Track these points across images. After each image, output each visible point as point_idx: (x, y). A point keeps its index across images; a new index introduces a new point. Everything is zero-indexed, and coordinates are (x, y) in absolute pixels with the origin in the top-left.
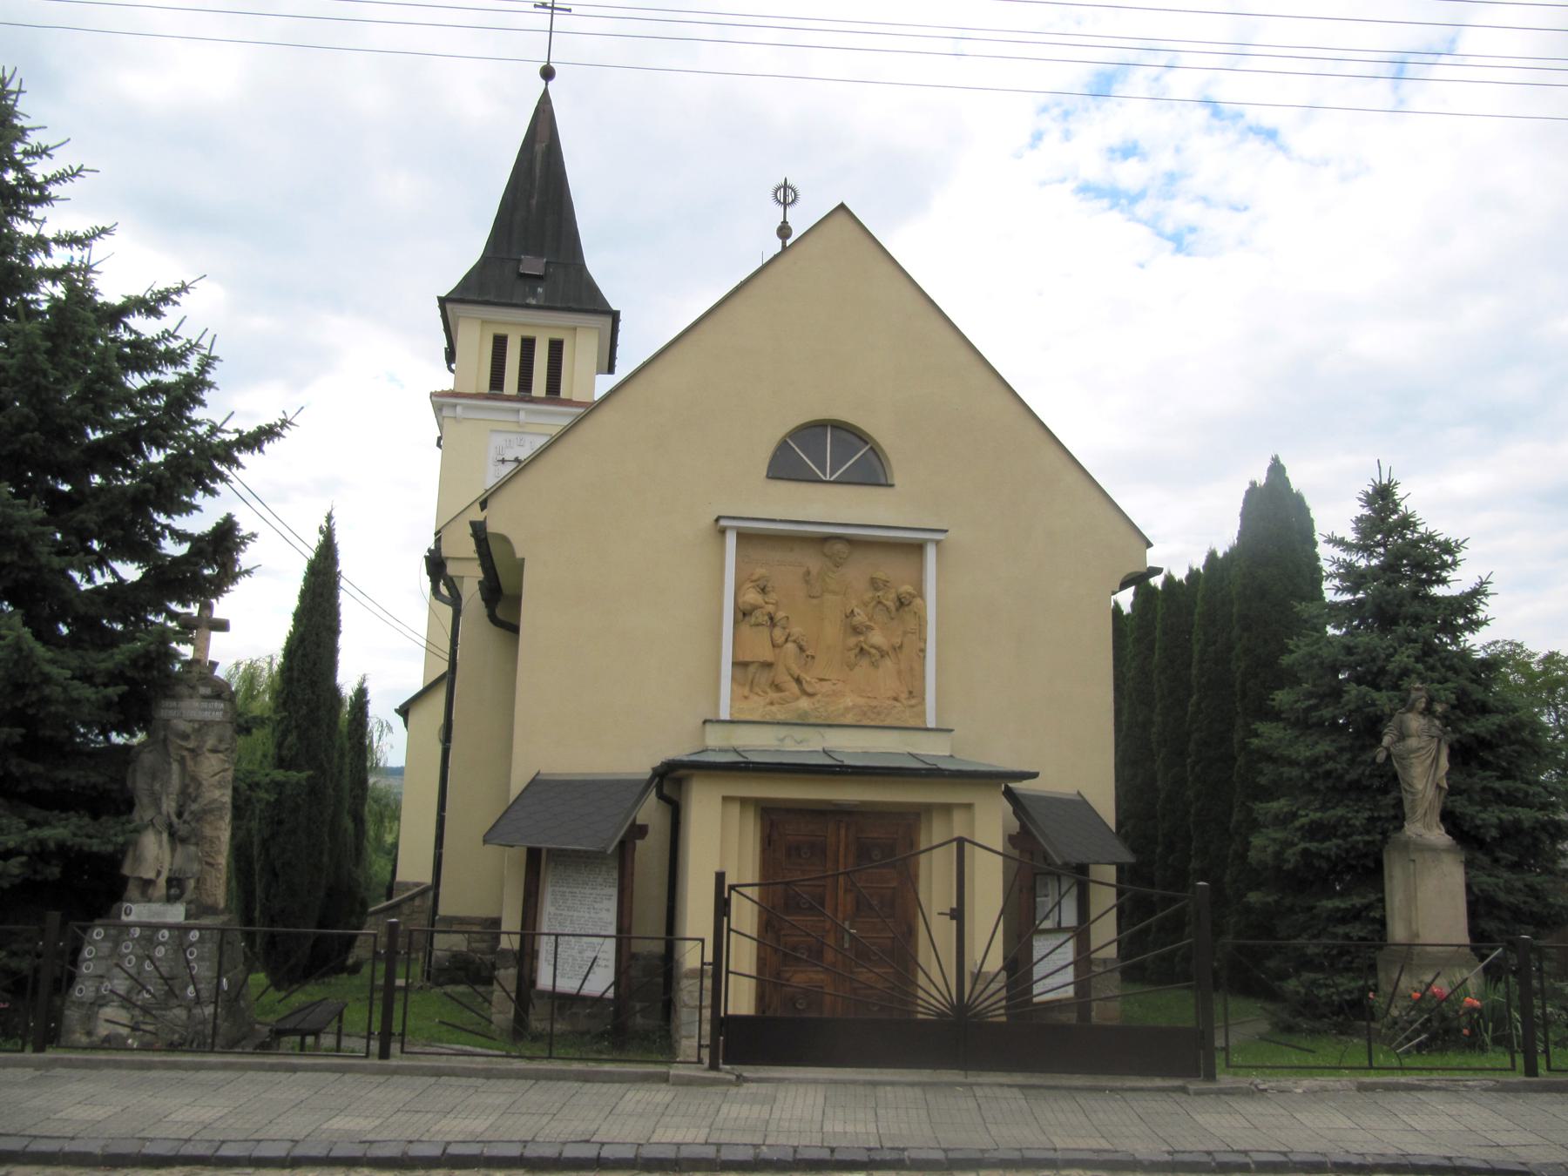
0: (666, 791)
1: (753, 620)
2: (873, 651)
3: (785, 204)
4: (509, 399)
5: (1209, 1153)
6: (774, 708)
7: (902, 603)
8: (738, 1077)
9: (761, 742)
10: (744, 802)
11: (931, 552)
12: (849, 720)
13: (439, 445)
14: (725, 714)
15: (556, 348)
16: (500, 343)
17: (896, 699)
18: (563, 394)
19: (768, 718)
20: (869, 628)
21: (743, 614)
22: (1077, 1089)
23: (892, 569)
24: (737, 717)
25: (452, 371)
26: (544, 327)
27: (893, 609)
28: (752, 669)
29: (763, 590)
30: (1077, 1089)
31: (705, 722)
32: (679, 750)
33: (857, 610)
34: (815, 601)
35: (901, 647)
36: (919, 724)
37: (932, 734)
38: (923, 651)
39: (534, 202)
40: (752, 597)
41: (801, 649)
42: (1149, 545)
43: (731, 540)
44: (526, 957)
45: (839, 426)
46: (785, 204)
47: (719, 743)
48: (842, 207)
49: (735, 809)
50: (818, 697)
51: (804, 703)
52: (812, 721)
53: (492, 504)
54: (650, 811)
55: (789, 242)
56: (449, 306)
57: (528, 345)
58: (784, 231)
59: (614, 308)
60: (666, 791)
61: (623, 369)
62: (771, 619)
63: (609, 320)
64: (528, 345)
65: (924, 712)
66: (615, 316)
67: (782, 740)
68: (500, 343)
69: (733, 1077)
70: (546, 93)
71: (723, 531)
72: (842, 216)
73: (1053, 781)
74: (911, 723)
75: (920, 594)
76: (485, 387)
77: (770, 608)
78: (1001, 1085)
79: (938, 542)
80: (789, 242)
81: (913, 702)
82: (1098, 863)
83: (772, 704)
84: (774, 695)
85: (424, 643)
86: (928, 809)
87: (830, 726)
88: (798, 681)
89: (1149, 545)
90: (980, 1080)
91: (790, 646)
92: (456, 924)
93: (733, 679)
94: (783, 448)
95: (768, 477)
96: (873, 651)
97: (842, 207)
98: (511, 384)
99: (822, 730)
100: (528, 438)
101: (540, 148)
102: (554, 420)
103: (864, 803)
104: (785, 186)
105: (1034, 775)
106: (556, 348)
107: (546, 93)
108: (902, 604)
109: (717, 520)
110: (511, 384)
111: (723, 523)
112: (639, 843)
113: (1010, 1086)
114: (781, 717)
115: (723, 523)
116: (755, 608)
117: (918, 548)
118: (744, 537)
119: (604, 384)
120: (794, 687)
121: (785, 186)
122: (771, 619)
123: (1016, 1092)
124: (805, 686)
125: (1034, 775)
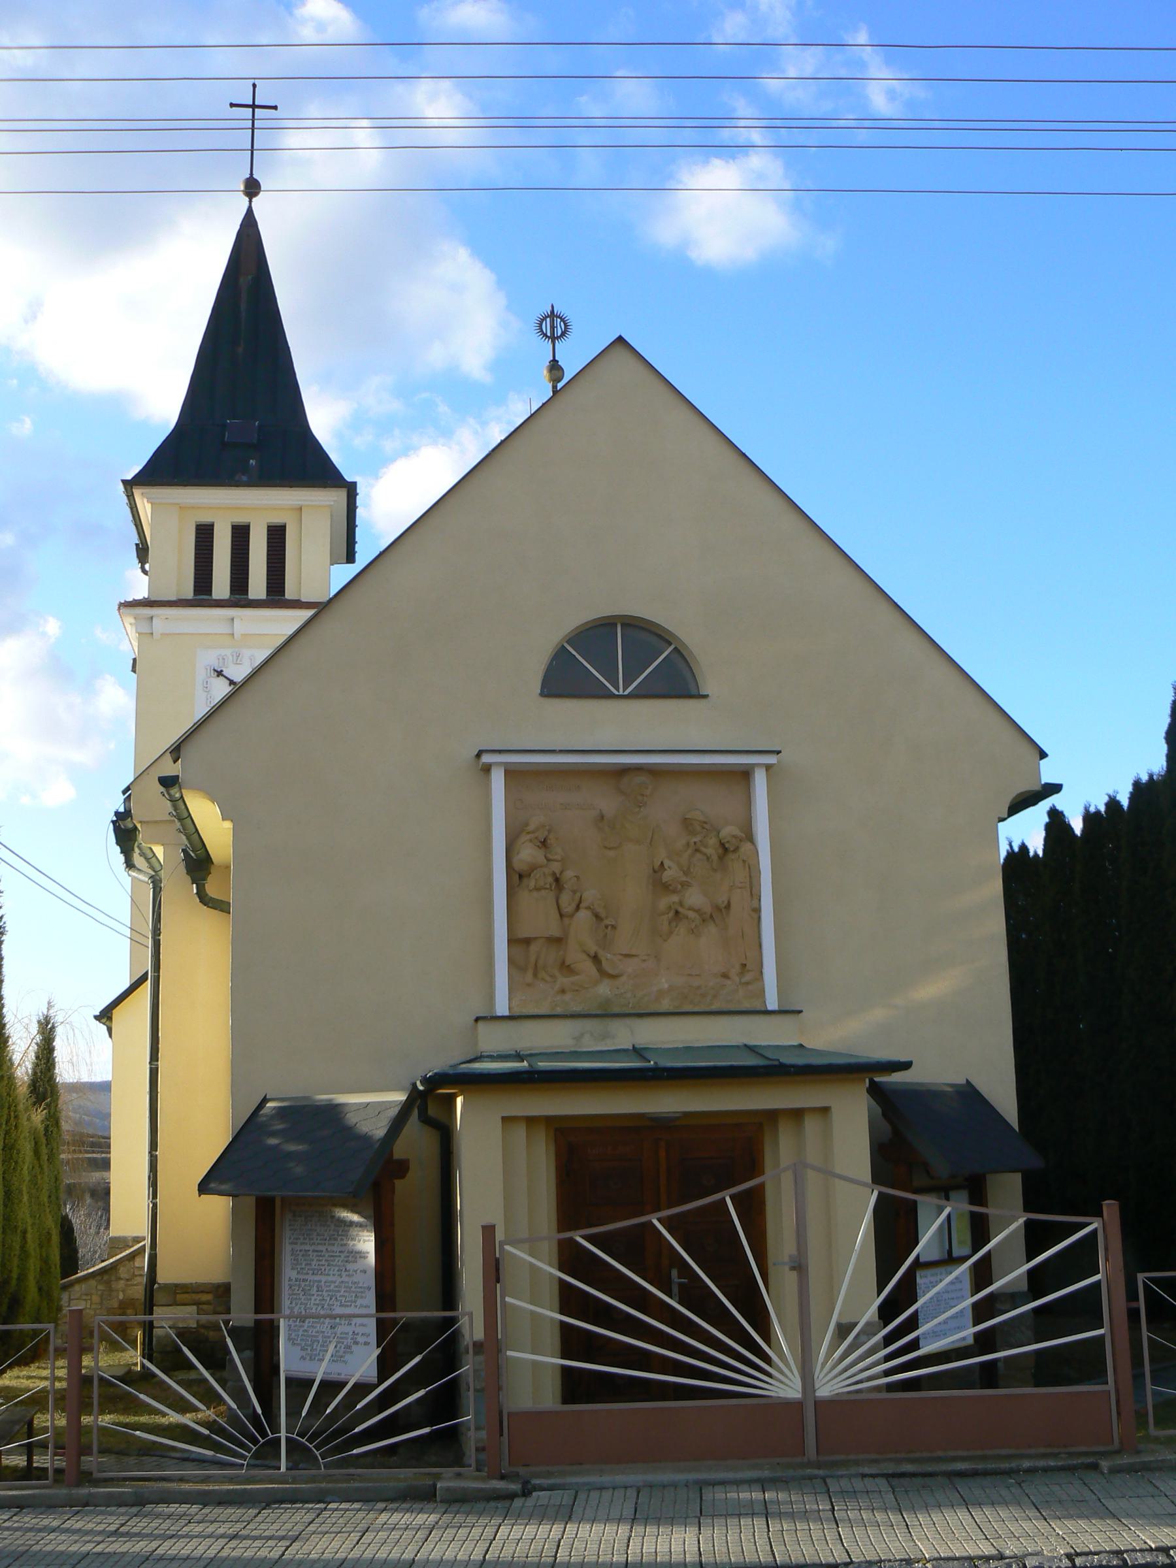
0: (432, 1111)
1: (532, 884)
2: (691, 914)
3: (553, 339)
4: (220, 604)
5: (1118, 1553)
6: (567, 997)
7: (725, 849)
8: (526, 1483)
9: (551, 1040)
10: (531, 1121)
11: (760, 781)
12: (666, 1005)
13: (134, 670)
14: (502, 1008)
15: (277, 535)
16: (205, 534)
17: (725, 976)
18: (289, 594)
19: (559, 1010)
20: (685, 885)
21: (517, 877)
22: (961, 1474)
23: (713, 804)
24: (517, 1011)
25: (145, 572)
26: (258, 505)
27: (715, 858)
28: (534, 948)
29: (544, 844)
30: (961, 1474)
31: (477, 1020)
32: (437, 1064)
33: (667, 863)
34: (611, 853)
35: (728, 906)
36: (758, 1006)
37: (773, 1018)
38: (758, 910)
39: (240, 350)
40: (528, 853)
41: (597, 916)
42: (1043, 755)
43: (498, 779)
44: (261, 1342)
45: (633, 625)
46: (553, 339)
47: (498, 1047)
48: (620, 340)
49: (520, 1132)
50: (624, 979)
51: (604, 989)
52: (616, 1010)
53: (188, 752)
54: (416, 1142)
55: (560, 385)
56: (137, 493)
57: (241, 534)
58: (555, 367)
59: (349, 478)
60: (432, 1111)
61: (364, 555)
62: (557, 880)
63: (341, 495)
64: (241, 534)
65: (762, 991)
66: (351, 490)
67: (578, 1039)
68: (205, 534)
69: (515, 1487)
70: (250, 212)
71: (487, 769)
72: (620, 351)
73: (933, 1069)
74: (746, 1005)
75: (750, 837)
76: (188, 592)
77: (556, 867)
78: (864, 1476)
79: (768, 767)
80: (560, 385)
81: (747, 977)
82: (996, 1172)
83: (563, 991)
84: (563, 981)
85: (128, 932)
86: (772, 1116)
87: (640, 1015)
88: (596, 959)
89: (1043, 755)
90: (606, 1479)
91: (583, 914)
92: (180, 1293)
93: (511, 961)
94: (560, 658)
95: (543, 694)
96: (691, 914)
97: (620, 340)
98: (221, 584)
99: (628, 1021)
100: (247, 653)
101: (245, 281)
102: (285, 622)
103: (687, 1115)
104: (552, 315)
105: (906, 1066)
106: (277, 535)
107: (250, 212)
108: (726, 850)
109: (479, 755)
110: (221, 584)
111: (486, 759)
112: (398, 1183)
113: (873, 1476)
114: (576, 1008)
115: (486, 759)
116: (533, 868)
117: (745, 775)
118: (513, 774)
119: (342, 574)
120: (589, 967)
121: (552, 315)
122: (557, 880)
123: (882, 1483)
124: (606, 965)
125: (906, 1066)
